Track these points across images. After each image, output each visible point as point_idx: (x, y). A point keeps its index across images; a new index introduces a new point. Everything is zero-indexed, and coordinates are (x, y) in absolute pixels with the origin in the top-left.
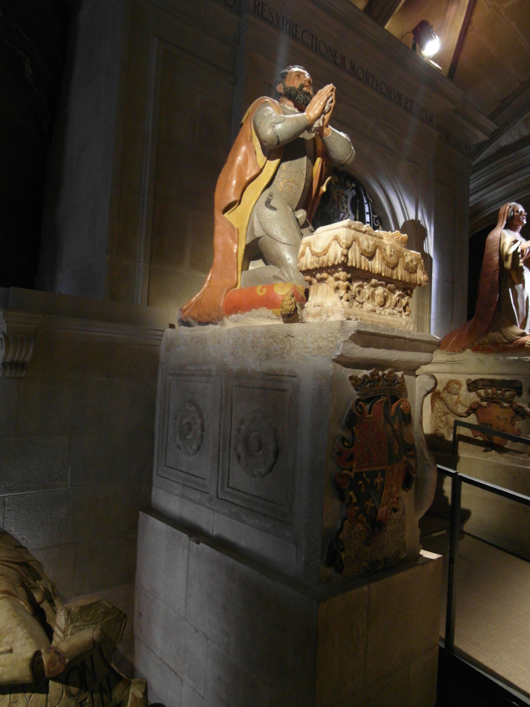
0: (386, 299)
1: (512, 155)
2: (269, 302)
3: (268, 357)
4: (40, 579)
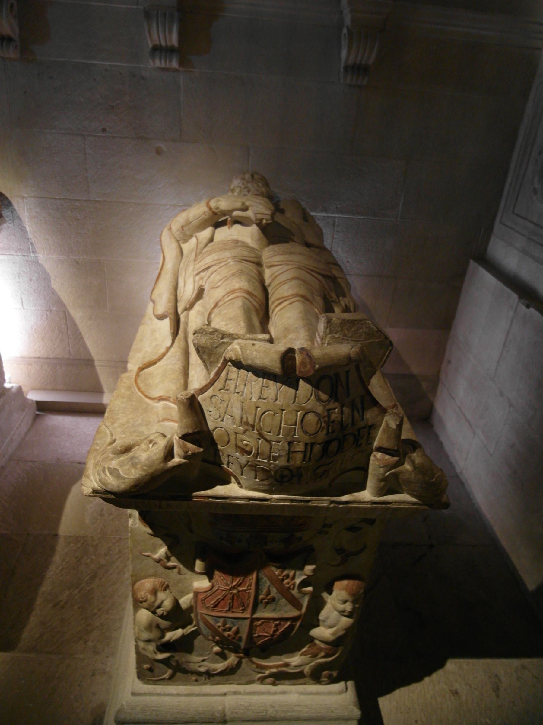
4: (344, 296)
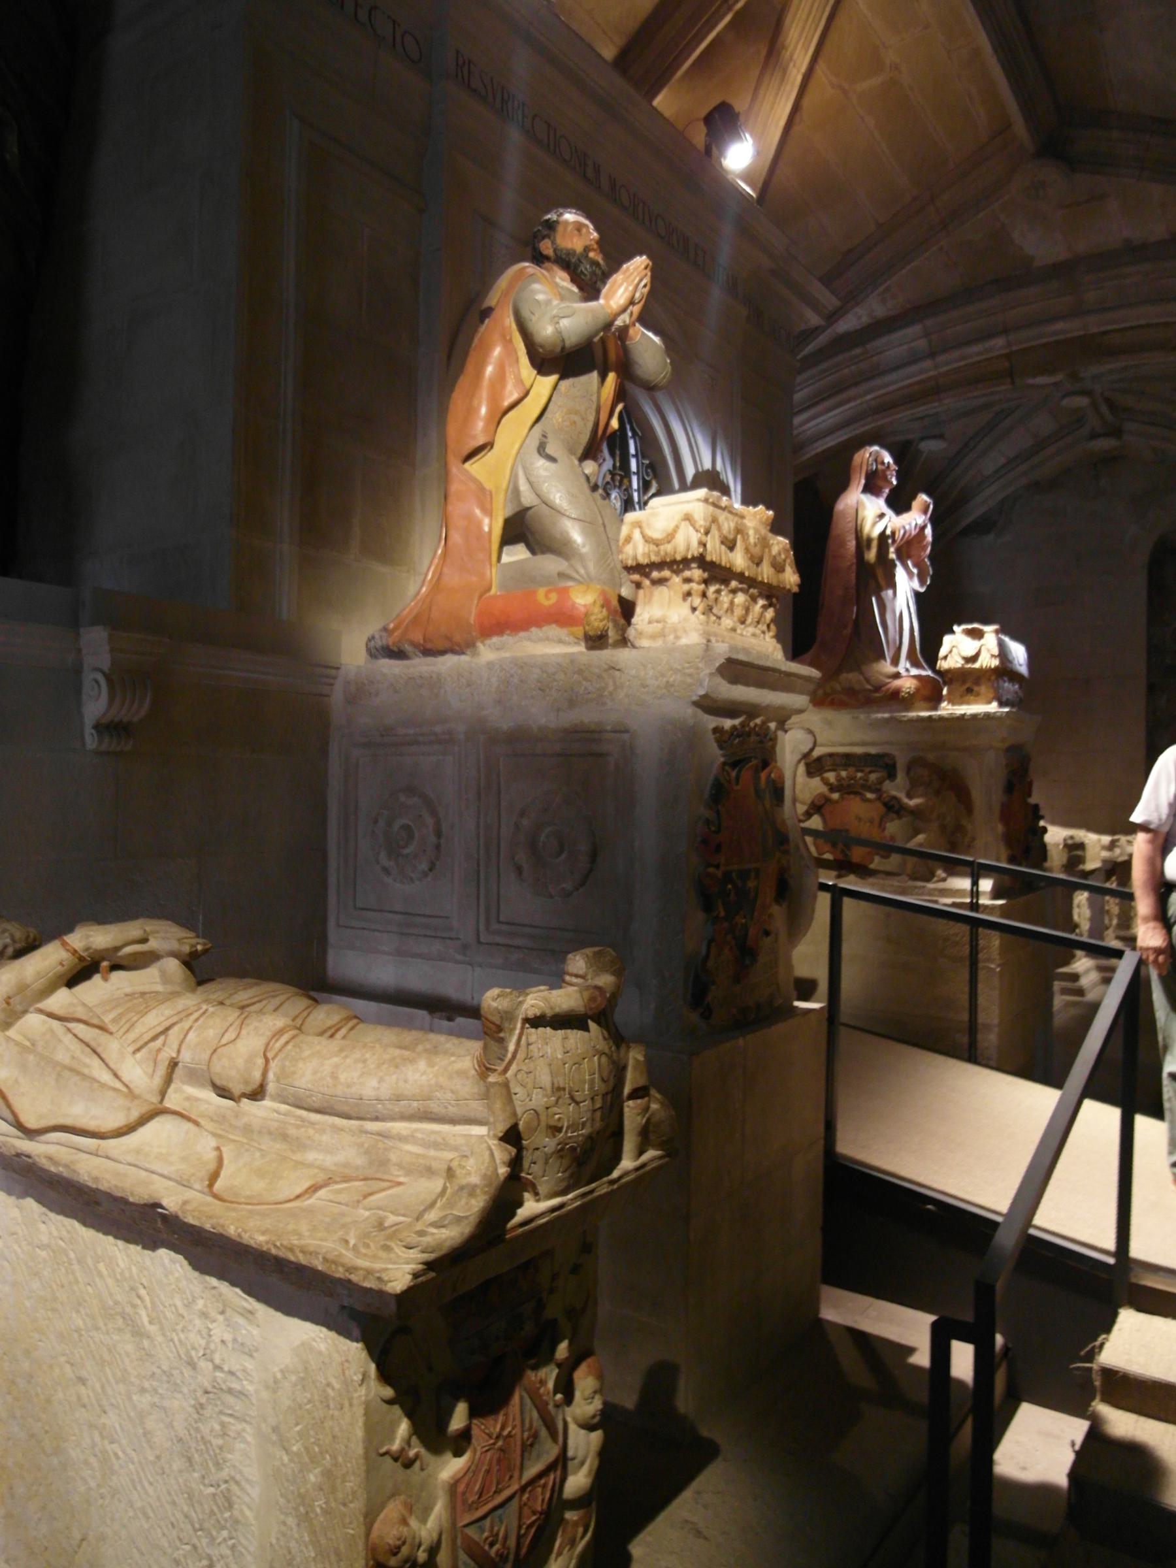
0: (747, 610)
1: (858, 351)
2: (563, 617)
3: (572, 704)
